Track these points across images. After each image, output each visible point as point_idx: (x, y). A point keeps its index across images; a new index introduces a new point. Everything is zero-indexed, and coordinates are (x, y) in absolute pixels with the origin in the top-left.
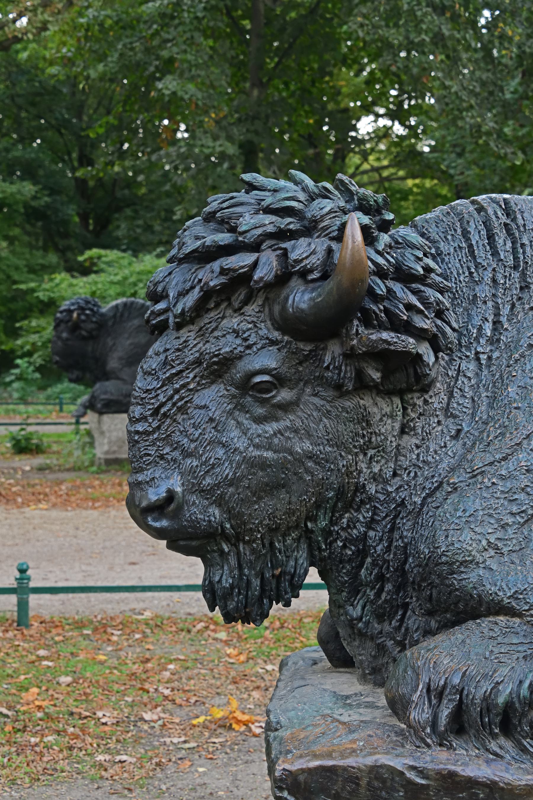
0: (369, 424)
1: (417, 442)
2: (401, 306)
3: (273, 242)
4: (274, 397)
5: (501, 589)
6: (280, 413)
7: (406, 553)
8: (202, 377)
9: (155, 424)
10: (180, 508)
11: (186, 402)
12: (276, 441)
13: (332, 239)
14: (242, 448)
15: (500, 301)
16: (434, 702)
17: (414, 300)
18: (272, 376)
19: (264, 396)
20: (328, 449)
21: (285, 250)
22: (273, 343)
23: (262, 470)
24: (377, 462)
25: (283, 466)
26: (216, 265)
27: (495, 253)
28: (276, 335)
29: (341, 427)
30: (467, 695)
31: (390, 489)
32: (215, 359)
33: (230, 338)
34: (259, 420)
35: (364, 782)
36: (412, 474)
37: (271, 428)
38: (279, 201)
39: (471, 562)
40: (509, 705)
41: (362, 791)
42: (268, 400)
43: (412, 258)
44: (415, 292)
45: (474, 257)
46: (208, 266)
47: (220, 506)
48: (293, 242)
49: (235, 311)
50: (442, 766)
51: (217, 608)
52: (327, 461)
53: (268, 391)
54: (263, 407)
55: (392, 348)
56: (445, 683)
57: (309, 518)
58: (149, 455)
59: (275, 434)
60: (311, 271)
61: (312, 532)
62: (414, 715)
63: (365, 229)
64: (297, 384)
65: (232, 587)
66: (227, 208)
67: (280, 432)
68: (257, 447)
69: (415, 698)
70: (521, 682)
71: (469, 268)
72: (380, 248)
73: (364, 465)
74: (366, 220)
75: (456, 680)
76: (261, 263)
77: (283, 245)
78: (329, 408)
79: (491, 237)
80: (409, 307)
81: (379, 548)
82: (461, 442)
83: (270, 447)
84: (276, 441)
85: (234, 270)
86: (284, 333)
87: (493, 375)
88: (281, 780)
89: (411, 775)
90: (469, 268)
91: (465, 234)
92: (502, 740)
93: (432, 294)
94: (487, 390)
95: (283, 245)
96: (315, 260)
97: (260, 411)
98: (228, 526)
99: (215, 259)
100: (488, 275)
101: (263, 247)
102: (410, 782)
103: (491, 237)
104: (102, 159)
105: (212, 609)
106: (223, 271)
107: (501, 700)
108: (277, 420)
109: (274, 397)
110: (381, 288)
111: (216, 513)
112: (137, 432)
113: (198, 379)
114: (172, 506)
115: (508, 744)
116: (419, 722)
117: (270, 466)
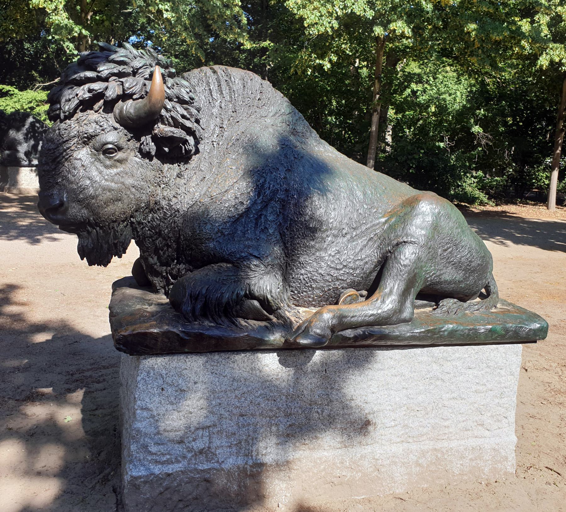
0: (163, 173)
1: (185, 182)
2: (179, 115)
3: (116, 78)
4: (115, 156)
5: (224, 251)
6: (118, 164)
7: (179, 234)
8: (78, 144)
9: (53, 167)
10: (67, 209)
11: (70, 156)
12: (116, 178)
13: (146, 79)
14: (99, 181)
15: (223, 117)
16: (193, 302)
17: (185, 113)
18: (115, 145)
19: (111, 155)
20: (142, 183)
21: (122, 82)
22: (116, 129)
23: (109, 192)
24: (166, 190)
25: (120, 191)
26: (86, 86)
27: (222, 93)
28: (117, 125)
29: (148, 173)
30: (209, 298)
31: (172, 204)
32: (86, 135)
33: (94, 125)
34: (107, 167)
35: (160, 339)
36: (183, 197)
37: (114, 171)
38: (118, 57)
39: (211, 238)
40: (228, 303)
41: (159, 343)
42: (112, 157)
43: (185, 92)
44: (186, 109)
45: (212, 95)
46: (82, 87)
47: (87, 208)
48: (126, 78)
49: (96, 112)
50: (197, 331)
51: (85, 258)
52: (141, 189)
53: (112, 153)
54: (110, 161)
55: (175, 135)
56: (199, 293)
57: (132, 216)
58: (50, 182)
59: (116, 174)
60: (134, 94)
61: (134, 223)
62: (184, 307)
63: (163, 75)
64: (127, 150)
65: (93, 248)
66: (92, 58)
67: (118, 174)
68: (106, 180)
69: (185, 300)
70: (233, 292)
71: (209, 100)
72: (169, 86)
73: (159, 192)
74: (162, 70)
75: (204, 291)
76: (109, 88)
77: (121, 80)
78: (142, 163)
79: (219, 86)
80: (183, 117)
81: (166, 231)
82: (205, 183)
83: (112, 181)
84: (116, 178)
85: (96, 91)
86: (121, 126)
87: (220, 153)
88: (120, 340)
89: (181, 335)
90: (209, 100)
91: (208, 84)
92: (223, 318)
93: (194, 111)
94: (217, 159)
95: (121, 80)
96: (137, 89)
97: (108, 162)
98: (92, 219)
99: (85, 84)
100: (217, 104)
101: (110, 79)
102: (182, 339)
103: (219, 86)
104: (59, 18)
105: (82, 259)
106: (90, 91)
107: (224, 300)
108: (116, 167)
109: (115, 156)
110: (169, 105)
111: (85, 212)
112: (44, 171)
113: (76, 145)
114: (63, 208)
115: (226, 320)
116: (271, 292)
117: (113, 190)
